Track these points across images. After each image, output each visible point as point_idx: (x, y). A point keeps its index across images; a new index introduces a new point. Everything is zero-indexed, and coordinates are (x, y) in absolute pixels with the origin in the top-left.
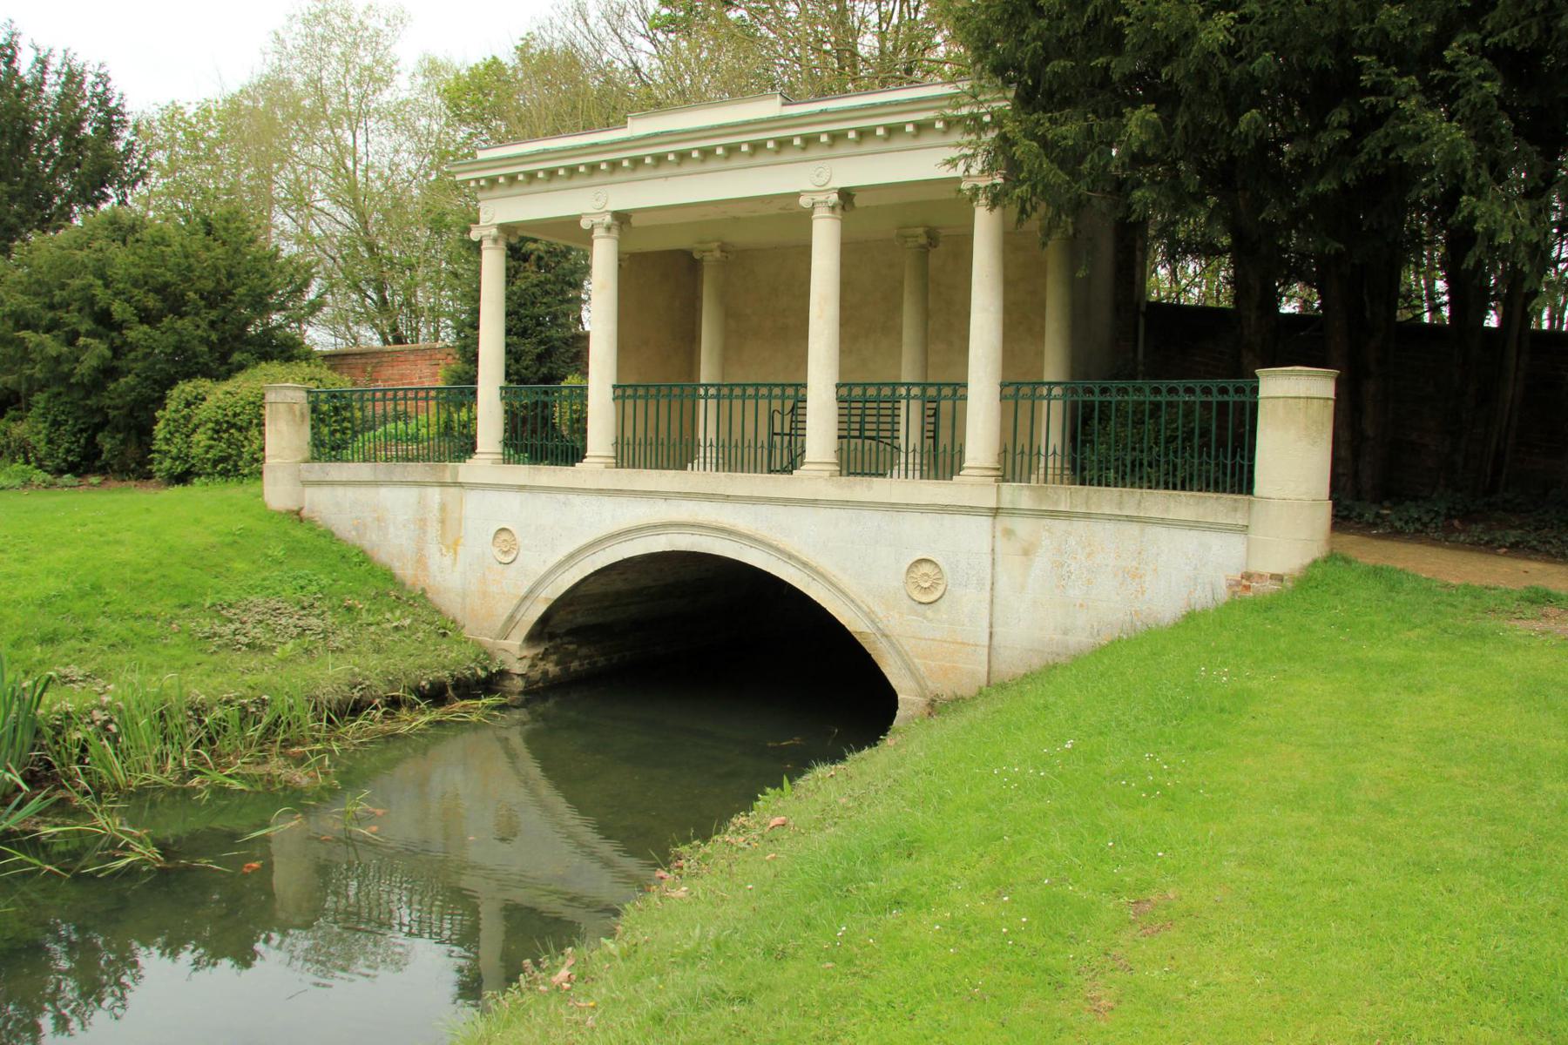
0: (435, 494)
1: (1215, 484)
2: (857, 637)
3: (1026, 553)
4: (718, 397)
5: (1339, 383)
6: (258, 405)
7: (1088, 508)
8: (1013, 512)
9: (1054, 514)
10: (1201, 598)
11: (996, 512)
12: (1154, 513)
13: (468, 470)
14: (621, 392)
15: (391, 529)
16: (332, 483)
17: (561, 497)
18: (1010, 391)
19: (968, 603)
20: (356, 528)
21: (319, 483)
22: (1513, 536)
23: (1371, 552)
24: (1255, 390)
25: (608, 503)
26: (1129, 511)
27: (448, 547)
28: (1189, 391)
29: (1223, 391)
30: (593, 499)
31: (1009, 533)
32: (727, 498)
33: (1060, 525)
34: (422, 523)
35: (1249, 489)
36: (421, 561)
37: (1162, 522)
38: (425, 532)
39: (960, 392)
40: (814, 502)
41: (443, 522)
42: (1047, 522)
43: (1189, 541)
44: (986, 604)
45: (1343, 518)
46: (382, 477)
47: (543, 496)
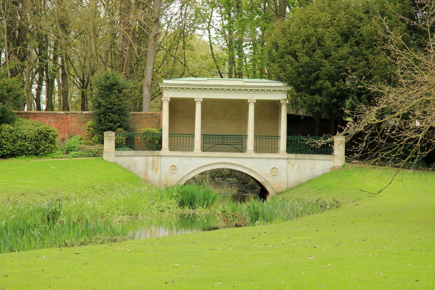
0: (151, 158)
2: (261, 183)
3: (293, 166)
6: (332, 143)
7: (304, 157)
8: (290, 159)
9: (298, 159)
10: (325, 171)
11: (288, 159)
13: (161, 153)
15: (138, 167)
17: (190, 158)
18: (256, 137)
19: (283, 176)
20: (128, 167)
21: (119, 156)
25: (203, 159)
27: (154, 171)
28: (291, 138)
29: (291, 138)
30: (199, 159)
31: (290, 162)
32: (233, 157)
33: (299, 161)
34: (147, 165)
36: (146, 174)
38: (147, 167)
39: (193, 136)
40: (252, 158)
41: (153, 165)
42: (297, 160)
43: (322, 163)
44: (286, 175)
45: (347, 161)
46: (136, 154)
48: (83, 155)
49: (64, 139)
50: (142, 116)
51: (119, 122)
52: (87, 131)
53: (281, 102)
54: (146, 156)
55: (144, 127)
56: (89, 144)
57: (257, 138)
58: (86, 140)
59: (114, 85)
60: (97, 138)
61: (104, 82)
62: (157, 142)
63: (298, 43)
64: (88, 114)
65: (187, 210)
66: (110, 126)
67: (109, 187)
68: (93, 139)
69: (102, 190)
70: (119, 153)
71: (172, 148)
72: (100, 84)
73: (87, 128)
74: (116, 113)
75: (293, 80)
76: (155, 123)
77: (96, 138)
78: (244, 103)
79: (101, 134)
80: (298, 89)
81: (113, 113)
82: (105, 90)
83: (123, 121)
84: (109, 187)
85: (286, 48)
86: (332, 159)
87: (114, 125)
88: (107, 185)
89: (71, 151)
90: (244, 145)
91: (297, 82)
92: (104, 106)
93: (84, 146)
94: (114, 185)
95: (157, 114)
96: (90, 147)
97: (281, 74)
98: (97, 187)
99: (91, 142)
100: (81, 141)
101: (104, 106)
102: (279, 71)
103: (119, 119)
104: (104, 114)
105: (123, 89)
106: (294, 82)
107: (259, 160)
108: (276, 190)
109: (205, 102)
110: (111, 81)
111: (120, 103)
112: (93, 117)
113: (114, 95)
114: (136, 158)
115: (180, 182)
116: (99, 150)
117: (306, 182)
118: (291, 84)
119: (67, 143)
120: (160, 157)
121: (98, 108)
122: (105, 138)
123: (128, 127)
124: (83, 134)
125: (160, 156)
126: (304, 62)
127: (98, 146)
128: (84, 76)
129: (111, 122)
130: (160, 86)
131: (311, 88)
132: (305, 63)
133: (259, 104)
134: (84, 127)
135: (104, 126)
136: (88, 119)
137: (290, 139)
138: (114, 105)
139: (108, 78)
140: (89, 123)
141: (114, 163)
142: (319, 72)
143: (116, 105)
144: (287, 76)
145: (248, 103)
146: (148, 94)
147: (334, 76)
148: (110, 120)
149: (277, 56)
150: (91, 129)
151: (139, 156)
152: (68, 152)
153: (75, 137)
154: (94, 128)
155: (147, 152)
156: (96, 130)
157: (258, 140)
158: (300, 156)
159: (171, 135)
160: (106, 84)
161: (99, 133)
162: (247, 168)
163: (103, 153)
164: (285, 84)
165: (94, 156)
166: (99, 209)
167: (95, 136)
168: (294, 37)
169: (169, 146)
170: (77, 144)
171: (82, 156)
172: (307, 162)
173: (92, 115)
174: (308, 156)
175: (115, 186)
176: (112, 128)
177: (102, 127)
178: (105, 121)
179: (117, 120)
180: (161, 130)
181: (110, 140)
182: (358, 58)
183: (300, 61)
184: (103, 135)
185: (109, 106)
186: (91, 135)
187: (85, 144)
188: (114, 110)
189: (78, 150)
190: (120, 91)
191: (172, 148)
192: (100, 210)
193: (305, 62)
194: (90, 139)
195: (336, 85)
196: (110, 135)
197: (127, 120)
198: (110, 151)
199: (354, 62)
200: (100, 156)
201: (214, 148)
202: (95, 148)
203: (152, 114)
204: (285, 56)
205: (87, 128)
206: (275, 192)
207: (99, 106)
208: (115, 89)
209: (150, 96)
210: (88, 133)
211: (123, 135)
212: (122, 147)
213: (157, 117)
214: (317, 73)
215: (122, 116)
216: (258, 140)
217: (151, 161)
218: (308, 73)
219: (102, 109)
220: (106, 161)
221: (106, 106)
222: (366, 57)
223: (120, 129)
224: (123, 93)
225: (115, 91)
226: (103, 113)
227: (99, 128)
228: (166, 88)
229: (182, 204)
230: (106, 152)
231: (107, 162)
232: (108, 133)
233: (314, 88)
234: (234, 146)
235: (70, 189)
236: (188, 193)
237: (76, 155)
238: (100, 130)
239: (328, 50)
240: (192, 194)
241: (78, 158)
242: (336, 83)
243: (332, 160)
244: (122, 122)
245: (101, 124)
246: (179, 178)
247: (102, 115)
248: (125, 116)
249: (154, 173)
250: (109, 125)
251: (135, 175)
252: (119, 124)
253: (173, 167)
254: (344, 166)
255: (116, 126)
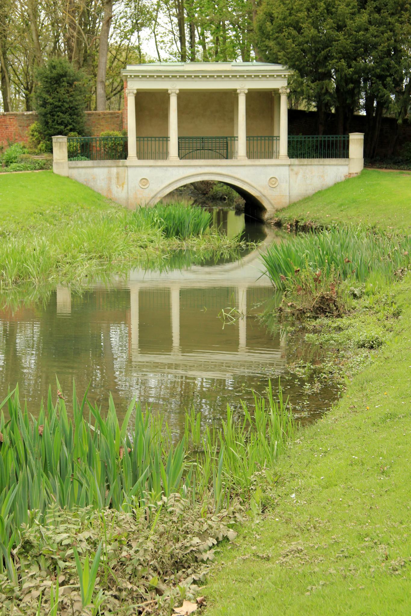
0: (114, 170)
1: (344, 157)
4: (269, 140)
5: (365, 136)
9: (303, 165)
10: (338, 180)
11: (290, 165)
12: (305, 163)
13: (127, 162)
14: (166, 139)
15: (98, 181)
16: (78, 168)
17: (165, 168)
18: (248, 139)
19: (284, 187)
22: (385, 166)
23: (370, 170)
24: (348, 137)
26: (321, 163)
27: (120, 186)
28: (333, 137)
29: (329, 137)
30: (176, 169)
31: (292, 170)
32: (219, 166)
33: (304, 167)
34: (110, 179)
35: (347, 157)
36: (109, 190)
37: (329, 165)
38: (111, 182)
39: (278, 138)
40: (244, 166)
41: (118, 178)
42: (301, 167)
43: (335, 168)
45: (366, 165)
46: (96, 165)
47: (158, 168)
48: (27, 167)
49: (2, 148)
50: (99, 116)
51: (70, 124)
52: (31, 137)
53: (280, 91)
54: (108, 167)
55: (103, 130)
56: (34, 153)
57: (250, 140)
58: (30, 148)
59: (62, 76)
60: (44, 145)
61: (49, 72)
62: (120, 148)
63: (301, 11)
64: (31, 115)
65: (175, 242)
66: (59, 130)
67: (63, 212)
68: (39, 146)
69: (54, 217)
70: (73, 163)
71: (141, 155)
72: (45, 75)
73: (31, 133)
74: (66, 112)
75: (296, 62)
76: (115, 125)
77: (42, 145)
78: (233, 95)
79: (49, 141)
80: (302, 73)
81: (63, 113)
82: (50, 83)
83: (76, 123)
84: (63, 212)
85: (284, 19)
86: (347, 163)
87: (65, 127)
88: (60, 209)
89: (11, 162)
90: (229, 150)
91: (302, 63)
92: (51, 104)
93: (28, 155)
94: (70, 208)
95: (118, 113)
96: (36, 158)
97: (279, 53)
98: (47, 212)
99: (36, 151)
100: (24, 149)
101: (51, 104)
102: (278, 49)
103: (70, 121)
104: (52, 114)
105: (74, 80)
106: (297, 63)
107: (254, 168)
108: (275, 206)
109: (183, 95)
110: (59, 70)
111: (72, 99)
112: (38, 119)
113: (63, 89)
114: (96, 170)
115: (154, 199)
116: (47, 161)
117: (314, 195)
118: (293, 67)
119: (6, 153)
120: (126, 168)
121: (43, 107)
122: (54, 144)
123: (83, 130)
124: (27, 140)
125: (127, 166)
126: (310, 35)
127: (46, 156)
128: (27, 83)
129: (61, 124)
130: (123, 74)
131: (320, 70)
132: (313, 37)
133: (252, 95)
134: (26, 132)
135: (52, 130)
136: (31, 121)
137: (291, 139)
138: (64, 102)
139: (54, 67)
140: (33, 126)
141: (68, 177)
142: (330, 48)
143: (67, 103)
144: (289, 56)
145: (238, 94)
146: (102, 92)
147: (350, 53)
148: (59, 121)
149: (272, 30)
150: (36, 133)
151: (99, 167)
152: (7, 163)
153: (16, 144)
154: (40, 133)
155: (109, 162)
156: (42, 135)
157: (251, 142)
158: (305, 161)
159: (139, 138)
160: (52, 75)
161: (47, 139)
162: (238, 179)
163: (53, 165)
164: (285, 67)
165: (42, 168)
166: (52, 253)
167: (42, 142)
168: (296, 4)
169: (137, 153)
170: (19, 154)
171: (26, 169)
172: (315, 168)
173: (37, 116)
174: (316, 161)
175: (71, 209)
176: (63, 132)
177: (49, 132)
178: (54, 124)
179: (68, 122)
180: (125, 134)
181: (61, 147)
182: (381, 29)
183: (305, 34)
184: (52, 142)
185: (56, 103)
186: (36, 142)
187: (29, 153)
188: (64, 109)
189: (20, 162)
190: (70, 84)
191: (141, 155)
192: (54, 255)
193: (312, 36)
194: (36, 147)
195: (353, 65)
196: (61, 140)
197: (81, 120)
198: (61, 161)
199: (376, 34)
200: (49, 168)
201: (191, 155)
202: (42, 158)
203: (111, 114)
204: (284, 30)
205: (31, 133)
206: (274, 208)
207: (45, 104)
208: (63, 81)
209: (105, 95)
210: (32, 139)
211: (77, 140)
212: (75, 156)
213: (118, 117)
214: (328, 49)
215: (75, 117)
216: (251, 142)
217: (115, 173)
218: (316, 51)
219: (49, 107)
220: (57, 175)
221: (53, 104)
222: (391, 26)
223: (72, 133)
224: (74, 86)
225: (64, 84)
226: (52, 112)
227: (46, 133)
228: (131, 76)
229: (167, 233)
230: (57, 163)
231: (58, 176)
232: (58, 138)
233: (323, 70)
234: (217, 151)
235: (8, 218)
236: (174, 217)
237: (18, 168)
238: (47, 135)
239: (341, 19)
240: (179, 219)
241: (20, 172)
242: (354, 63)
243: (347, 165)
244: (74, 124)
245: (48, 127)
246: (152, 195)
247: (49, 116)
248: (78, 116)
249: (120, 189)
250: (58, 129)
251: (95, 192)
252: (71, 126)
253: (144, 180)
254: (362, 173)
255: (67, 130)
